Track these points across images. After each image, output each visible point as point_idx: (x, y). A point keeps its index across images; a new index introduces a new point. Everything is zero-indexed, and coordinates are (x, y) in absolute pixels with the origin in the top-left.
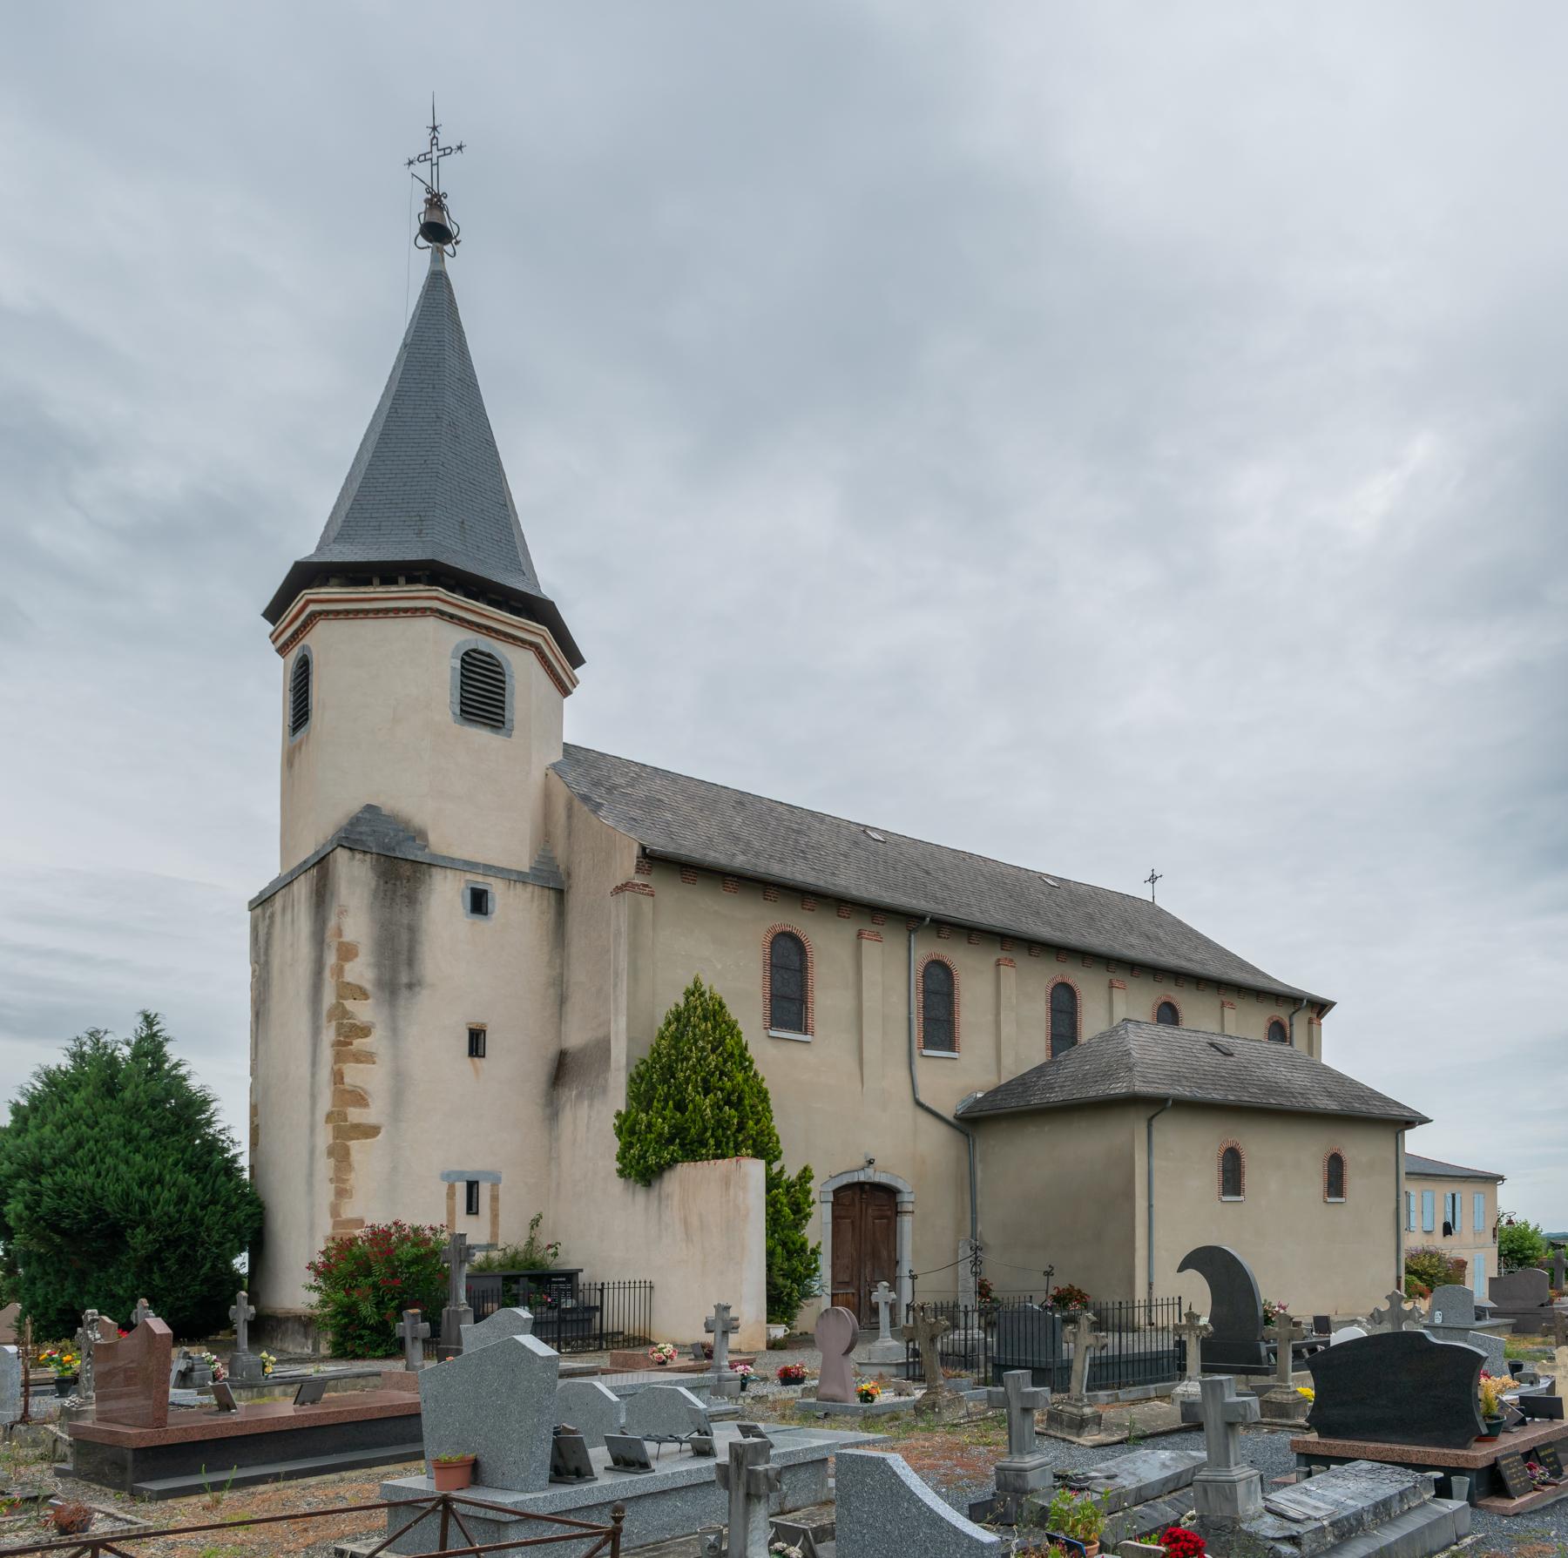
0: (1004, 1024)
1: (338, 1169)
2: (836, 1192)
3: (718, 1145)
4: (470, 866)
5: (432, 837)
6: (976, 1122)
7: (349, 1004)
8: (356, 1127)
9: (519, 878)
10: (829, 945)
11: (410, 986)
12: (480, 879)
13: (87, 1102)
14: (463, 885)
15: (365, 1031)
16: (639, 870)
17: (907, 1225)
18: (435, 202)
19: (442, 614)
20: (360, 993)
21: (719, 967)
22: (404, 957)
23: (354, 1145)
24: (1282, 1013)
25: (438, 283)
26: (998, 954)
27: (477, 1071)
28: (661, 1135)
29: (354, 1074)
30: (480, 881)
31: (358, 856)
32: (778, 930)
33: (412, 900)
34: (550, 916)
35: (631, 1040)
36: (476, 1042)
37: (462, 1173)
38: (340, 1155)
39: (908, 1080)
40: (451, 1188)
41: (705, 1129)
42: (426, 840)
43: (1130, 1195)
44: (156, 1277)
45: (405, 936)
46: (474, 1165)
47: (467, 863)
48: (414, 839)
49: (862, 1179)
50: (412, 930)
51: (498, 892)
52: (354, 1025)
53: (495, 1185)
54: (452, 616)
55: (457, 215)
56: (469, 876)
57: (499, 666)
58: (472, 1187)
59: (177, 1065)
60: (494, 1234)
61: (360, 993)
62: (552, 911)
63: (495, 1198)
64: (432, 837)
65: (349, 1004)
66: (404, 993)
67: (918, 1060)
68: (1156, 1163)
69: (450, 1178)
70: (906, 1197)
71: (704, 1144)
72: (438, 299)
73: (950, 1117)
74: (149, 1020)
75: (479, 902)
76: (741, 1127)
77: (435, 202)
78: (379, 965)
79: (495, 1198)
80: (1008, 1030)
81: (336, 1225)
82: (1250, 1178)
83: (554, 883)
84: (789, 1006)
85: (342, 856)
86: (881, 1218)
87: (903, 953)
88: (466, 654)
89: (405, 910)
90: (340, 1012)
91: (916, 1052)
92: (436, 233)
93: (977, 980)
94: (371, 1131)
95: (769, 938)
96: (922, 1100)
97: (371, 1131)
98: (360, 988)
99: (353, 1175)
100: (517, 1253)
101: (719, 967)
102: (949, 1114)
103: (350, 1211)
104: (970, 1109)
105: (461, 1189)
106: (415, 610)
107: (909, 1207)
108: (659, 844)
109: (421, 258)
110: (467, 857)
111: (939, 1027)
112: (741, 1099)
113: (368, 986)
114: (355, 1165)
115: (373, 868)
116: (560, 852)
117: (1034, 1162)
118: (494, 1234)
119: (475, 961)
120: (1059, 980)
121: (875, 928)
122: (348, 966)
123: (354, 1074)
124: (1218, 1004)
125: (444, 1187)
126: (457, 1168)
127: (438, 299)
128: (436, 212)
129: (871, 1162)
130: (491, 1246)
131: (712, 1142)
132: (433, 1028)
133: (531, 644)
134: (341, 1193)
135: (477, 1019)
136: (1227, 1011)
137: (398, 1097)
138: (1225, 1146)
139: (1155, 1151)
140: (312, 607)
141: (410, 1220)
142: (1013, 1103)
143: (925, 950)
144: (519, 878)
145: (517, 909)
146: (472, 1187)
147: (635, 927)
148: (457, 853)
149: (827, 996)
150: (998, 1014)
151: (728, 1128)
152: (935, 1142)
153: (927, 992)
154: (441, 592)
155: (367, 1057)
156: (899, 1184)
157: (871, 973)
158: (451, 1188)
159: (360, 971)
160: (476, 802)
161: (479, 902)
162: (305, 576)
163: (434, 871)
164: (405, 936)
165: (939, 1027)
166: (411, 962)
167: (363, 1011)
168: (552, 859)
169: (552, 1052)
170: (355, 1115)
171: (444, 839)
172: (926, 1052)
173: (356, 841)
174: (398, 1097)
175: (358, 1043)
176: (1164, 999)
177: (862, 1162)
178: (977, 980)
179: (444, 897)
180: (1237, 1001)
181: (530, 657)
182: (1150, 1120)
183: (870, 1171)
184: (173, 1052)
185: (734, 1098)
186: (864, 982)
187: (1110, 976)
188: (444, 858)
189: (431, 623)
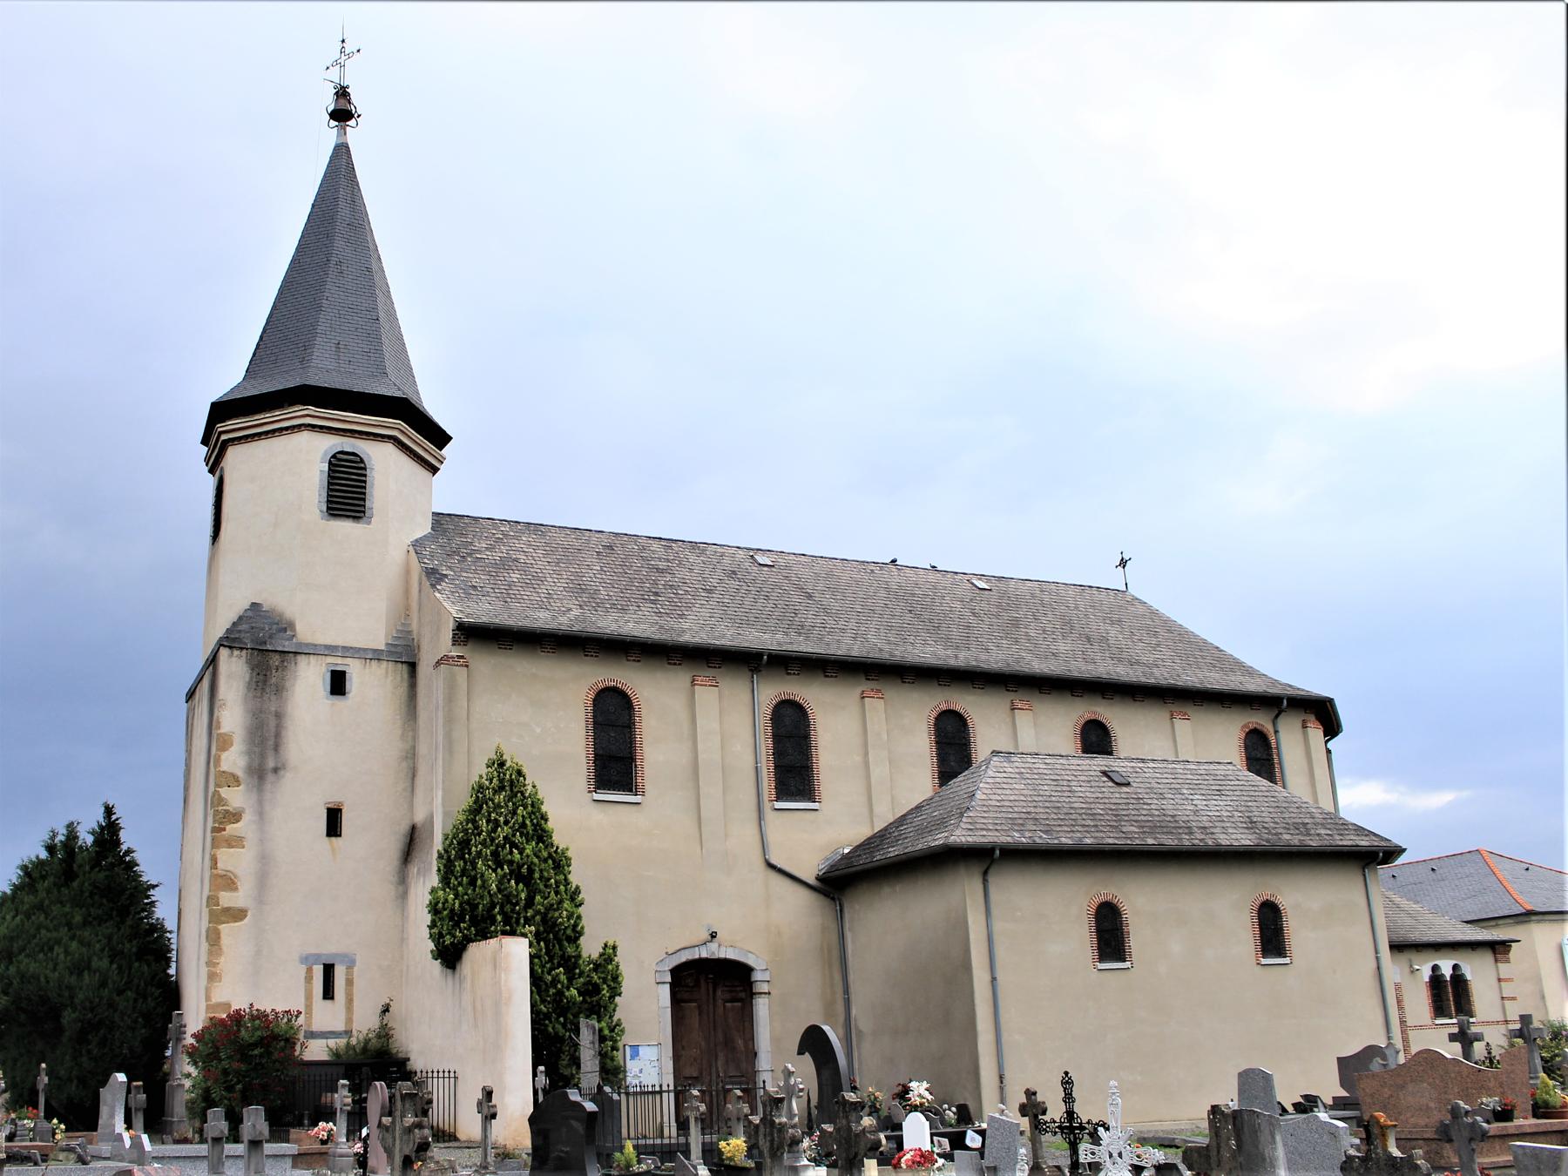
0: (875, 765)
1: (210, 953)
2: (675, 971)
3: (507, 921)
4: (331, 650)
5: (298, 628)
6: (840, 883)
7: (224, 792)
8: (227, 910)
9: (376, 656)
10: (658, 699)
11: (276, 770)
12: (339, 661)
13: (48, 892)
14: (324, 669)
15: (236, 817)
16: (455, 642)
17: (762, 1007)
18: (342, 93)
19: (313, 427)
20: (233, 780)
21: (538, 730)
22: (271, 742)
23: (225, 928)
24: (1261, 720)
25: (341, 154)
26: (866, 686)
27: (333, 850)
28: (452, 910)
29: (228, 859)
30: (339, 663)
31: (236, 652)
32: (601, 686)
33: (279, 690)
34: (403, 689)
35: (446, 814)
36: (334, 822)
37: (318, 956)
38: (214, 939)
39: (758, 837)
40: (309, 970)
41: (493, 906)
42: (294, 630)
43: (967, 967)
44: (84, 1059)
45: (272, 723)
46: (329, 949)
47: (327, 647)
48: (285, 630)
49: (704, 955)
50: (279, 716)
51: (357, 674)
52: (227, 812)
53: (350, 968)
54: (321, 427)
55: (358, 101)
56: (330, 660)
57: (362, 461)
58: (329, 970)
59: (129, 851)
60: (349, 1020)
61: (233, 780)
62: (405, 684)
63: (349, 982)
64: (300, 628)
65: (224, 792)
66: (270, 777)
67: (770, 816)
68: (998, 926)
69: (308, 961)
70: (757, 976)
71: (494, 921)
72: (341, 167)
73: (812, 881)
74: (109, 811)
75: (338, 684)
76: (530, 902)
77: (342, 93)
78: (249, 753)
79: (349, 982)
80: (879, 771)
81: (209, 1008)
82: (1137, 940)
83: (405, 658)
84: (615, 766)
85: (224, 652)
86: (732, 1000)
87: (746, 697)
88: (334, 456)
89: (273, 698)
90: (215, 801)
91: (767, 806)
92: (342, 115)
93: (836, 718)
94: (238, 915)
95: (592, 696)
96: (774, 861)
97: (238, 915)
98: (233, 775)
99: (222, 960)
100: (367, 1041)
101: (538, 730)
102: (809, 871)
103: (219, 996)
104: (833, 868)
105: (318, 971)
106: (293, 427)
107: (764, 988)
108: (484, 612)
109: (328, 135)
110: (328, 642)
111: (793, 772)
112: (531, 871)
113: (240, 773)
114: (224, 948)
115: (248, 662)
116: (414, 627)
117: (891, 923)
118: (349, 1020)
119: (336, 739)
120: (944, 707)
121: (711, 672)
122: (224, 756)
123: (228, 859)
124: (1168, 715)
125: (303, 969)
126: (313, 951)
127: (341, 167)
128: (342, 101)
129: (713, 936)
130: (348, 1033)
131: (499, 918)
132: (296, 807)
133: (390, 437)
134: (213, 977)
135: (334, 799)
136: (1178, 723)
137: (263, 879)
138: (1097, 901)
139: (995, 911)
140: (224, 437)
141: (265, 1005)
142: (863, 861)
143: (771, 691)
144: (376, 656)
145: (373, 685)
146: (329, 970)
147: (450, 699)
148: (322, 639)
149: (657, 749)
150: (866, 754)
151: (517, 904)
152: (797, 910)
153: (777, 738)
154: (312, 410)
155: (236, 842)
156: (750, 960)
157: (708, 721)
158: (309, 970)
159: (234, 760)
160: (345, 588)
161: (338, 684)
162: (221, 411)
163: (299, 658)
164: (272, 723)
165: (793, 772)
166: (277, 748)
167: (235, 797)
168: (410, 632)
169: (404, 828)
170: (227, 899)
171: (308, 630)
172: (779, 805)
173: (235, 640)
174: (263, 879)
175: (231, 829)
176: (1088, 716)
177: (706, 936)
178: (836, 718)
179: (309, 678)
180: (1191, 710)
181: (390, 448)
182: (985, 873)
183: (713, 946)
184: (127, 839)
185: (524, 870)
186: (701, 734)
187: (1012, 696)
188: (307, 645)
189: (305, 436)
